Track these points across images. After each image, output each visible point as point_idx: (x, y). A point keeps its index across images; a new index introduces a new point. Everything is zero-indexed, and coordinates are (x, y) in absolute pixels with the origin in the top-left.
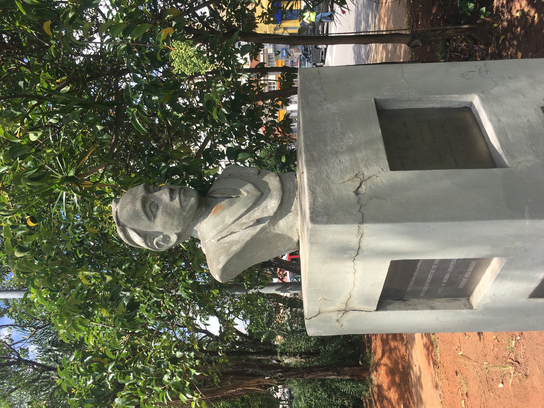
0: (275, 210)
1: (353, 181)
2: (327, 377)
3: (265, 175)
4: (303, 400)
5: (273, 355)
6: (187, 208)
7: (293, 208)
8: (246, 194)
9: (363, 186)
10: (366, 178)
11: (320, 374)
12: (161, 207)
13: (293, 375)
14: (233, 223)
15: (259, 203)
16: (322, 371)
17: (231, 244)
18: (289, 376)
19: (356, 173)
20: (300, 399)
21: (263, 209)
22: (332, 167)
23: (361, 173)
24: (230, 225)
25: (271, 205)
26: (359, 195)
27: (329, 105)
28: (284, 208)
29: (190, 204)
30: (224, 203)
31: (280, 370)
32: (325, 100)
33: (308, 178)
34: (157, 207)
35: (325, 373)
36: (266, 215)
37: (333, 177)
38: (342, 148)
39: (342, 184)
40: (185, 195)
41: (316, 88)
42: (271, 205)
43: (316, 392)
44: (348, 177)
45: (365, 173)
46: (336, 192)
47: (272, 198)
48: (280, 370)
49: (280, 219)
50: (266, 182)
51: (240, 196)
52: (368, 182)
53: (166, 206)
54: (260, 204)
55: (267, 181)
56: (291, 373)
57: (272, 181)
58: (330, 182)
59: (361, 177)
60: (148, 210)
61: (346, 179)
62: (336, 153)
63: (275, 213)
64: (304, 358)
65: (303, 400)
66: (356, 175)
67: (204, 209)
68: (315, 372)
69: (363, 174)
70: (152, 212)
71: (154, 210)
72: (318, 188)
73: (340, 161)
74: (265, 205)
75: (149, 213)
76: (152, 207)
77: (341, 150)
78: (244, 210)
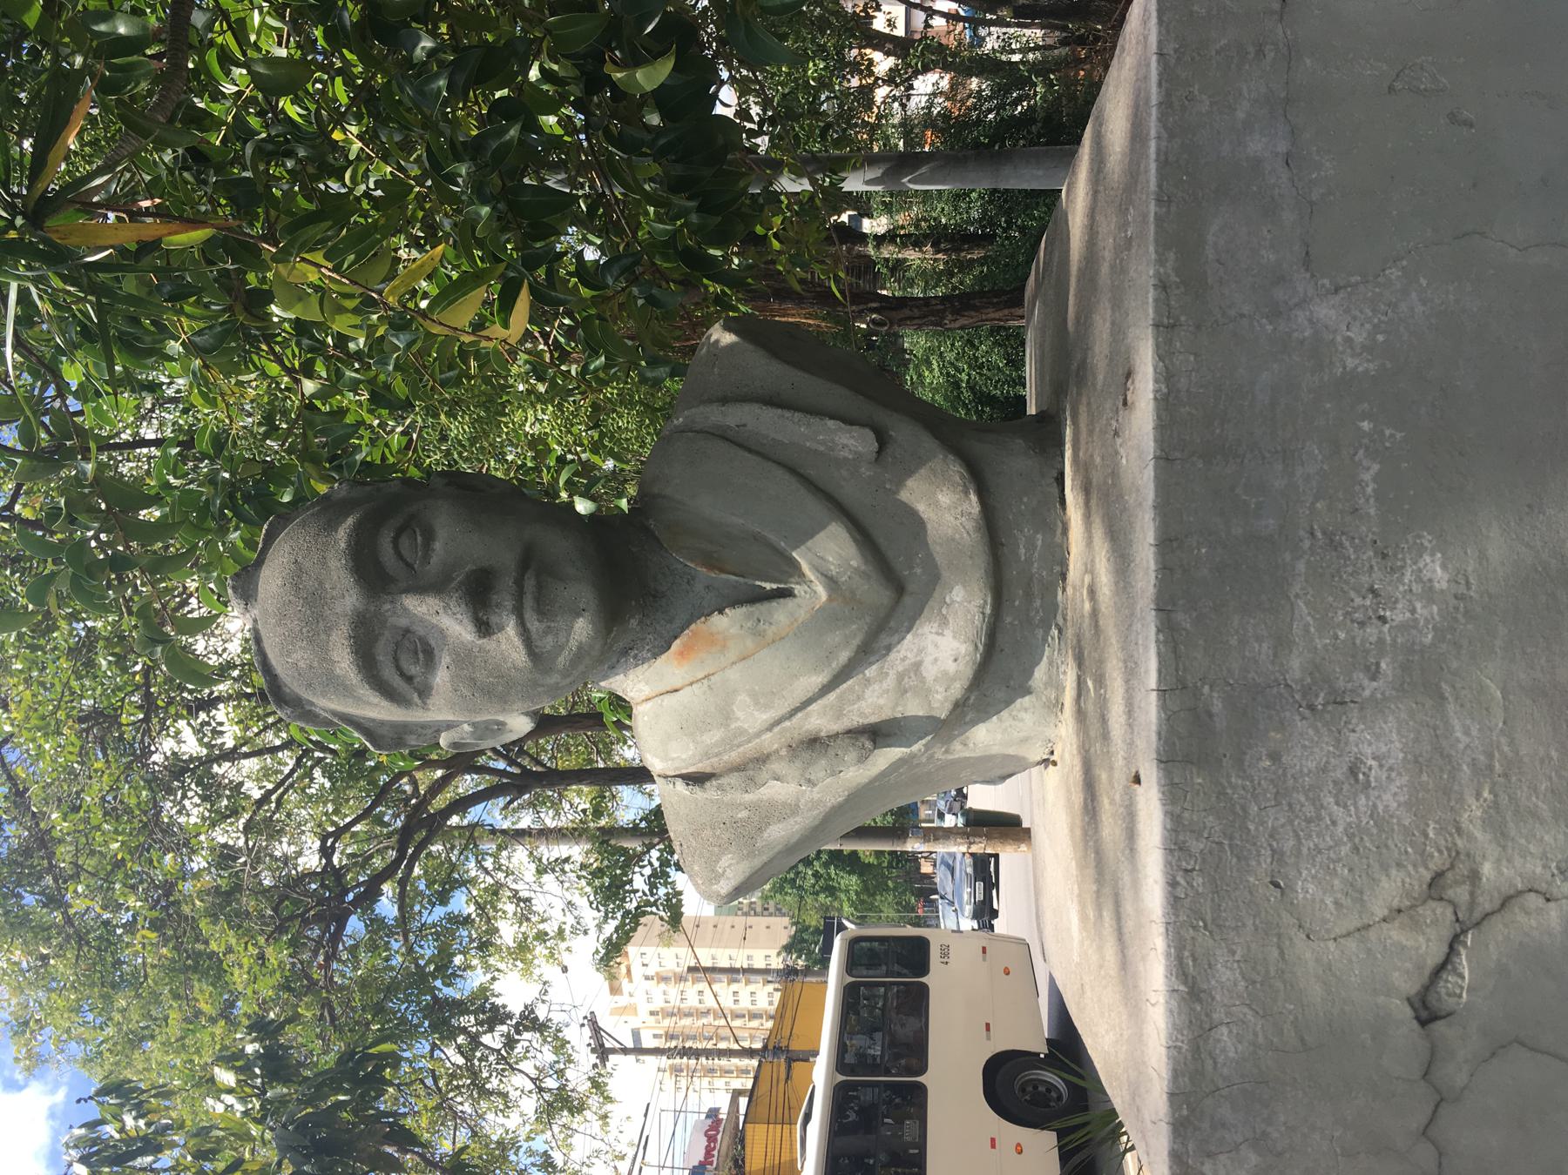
0: (957, 690)
1: (1416, 925)
2: (1011, 323)
3: (910, 473)
4: (935, 366)
5: (854, 244)
6: (562, 660)
7: (1040, 673)
8: (822, 592)
9: (1464, 962)
10: (1486, 904)
11: (992, 315)
12: (445, 659)
13: (911, 318)
14: (770, 728)
15: (884, 639)
16: (998, 307)
17: (768, 813)
18: (902, 322)
19: (1438, 861)
20: (929, 364)
21: (901, 677)
22: (1309, 810)
23: (1463, 868)
24: (758, 734)
25: (941, 649)
26: (1439, 1027)
27: (1326, 311)
28: (997, 674)
29: (573, 644)
30: (726, 623)
31: (874, 305)
32: (1307, 261)
33: (1172, 884)
34: (428, 656)
35: (1006, 312)
36: (913, 708)
37: (1306, 888)
38: (1374, 675)
39: (1351, 944)
40: (542, 612)
41: (1256, 145)
42: (941, 649)
43: (973, 345)
44: (1390, 889)
45: (1487, 869)
46: (1316, 991)
47: (944, 622)
48: (874, 305)
49: (974, 723)
50: (913, 514)
51: (798, 589)
52: (1497, 929)
53: (464, 658)
54: (889, 649)
55: (921, 507)
56: (906, 312)
57: (942, 506)
58: (1287, 919)
59: (1461, 893)
60: (389, 673)
61: (1380, 912)
62: (1330, 702)
63: (959, 706)
64: (945, 251)
65: (935, 366)
66: (1439, 876)
67: (633, 623)
68: (976, 309)
69: (1474, 876)
70: (409, 679)
71: (414, 670)
72: (1221, 956)
73: (1353, 771)
74: (912, 658)
75: (398, 682)
76: (405, 665)
77: (1369, 687)
78: (818, 680)
